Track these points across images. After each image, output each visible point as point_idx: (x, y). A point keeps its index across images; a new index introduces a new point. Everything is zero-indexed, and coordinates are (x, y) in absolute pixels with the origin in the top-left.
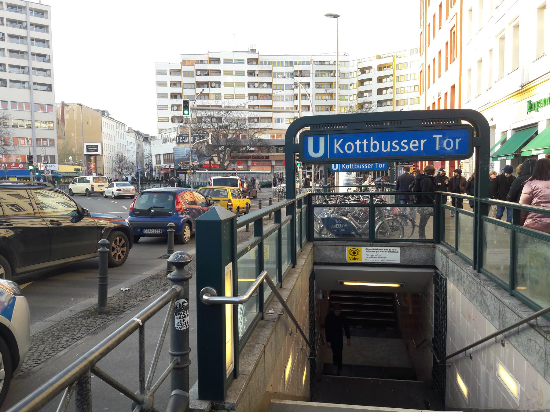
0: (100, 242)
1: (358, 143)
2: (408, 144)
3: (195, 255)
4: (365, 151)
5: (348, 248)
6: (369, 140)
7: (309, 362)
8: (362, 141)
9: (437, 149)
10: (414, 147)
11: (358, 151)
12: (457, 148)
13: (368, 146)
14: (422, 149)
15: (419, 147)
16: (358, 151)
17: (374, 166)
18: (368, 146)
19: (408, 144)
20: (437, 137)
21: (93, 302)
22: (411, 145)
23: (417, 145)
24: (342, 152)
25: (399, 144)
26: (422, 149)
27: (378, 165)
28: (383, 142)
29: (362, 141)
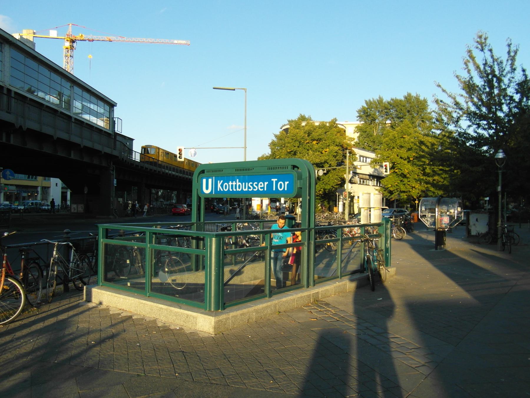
0: (65, 231)
1: (230, 183)
2: (257, 185)
3: (307, 357)
4: (235, 190)
5: (102, 227)
6: (236, 182)
7: (274, 297)
8: (232, 182)
9: (274, 189)
10: (261, 188)
11: (231, 190)
12: (286, 189)
13: (236, 185)
14: (265, 190)
15: (264, 188)
16: (231, 190)
17: (270, 185)
18: (236, 185)
19: (257, 185)
20: (274, 180)
21: (85, 326)
22: (259, 186)
23: (263, 186)
24: (222, 190)
25: (252, 185)
26: (265, 190)
27: (277, 183)
28: (244, 184)
29: (232, 182)
